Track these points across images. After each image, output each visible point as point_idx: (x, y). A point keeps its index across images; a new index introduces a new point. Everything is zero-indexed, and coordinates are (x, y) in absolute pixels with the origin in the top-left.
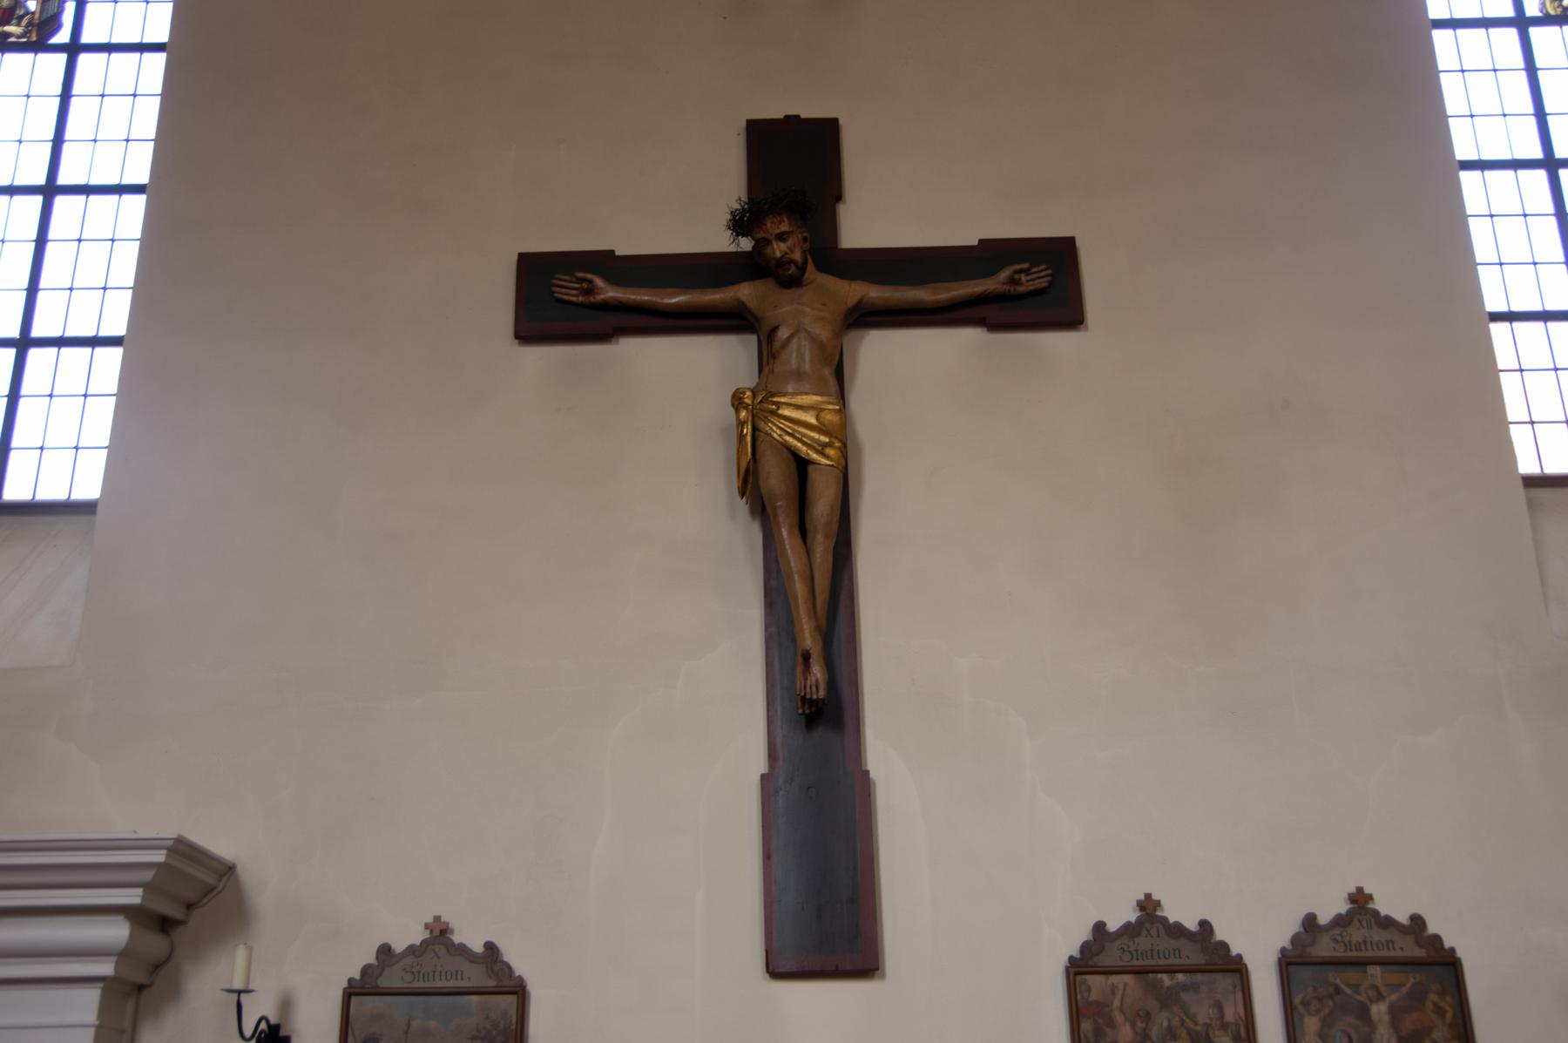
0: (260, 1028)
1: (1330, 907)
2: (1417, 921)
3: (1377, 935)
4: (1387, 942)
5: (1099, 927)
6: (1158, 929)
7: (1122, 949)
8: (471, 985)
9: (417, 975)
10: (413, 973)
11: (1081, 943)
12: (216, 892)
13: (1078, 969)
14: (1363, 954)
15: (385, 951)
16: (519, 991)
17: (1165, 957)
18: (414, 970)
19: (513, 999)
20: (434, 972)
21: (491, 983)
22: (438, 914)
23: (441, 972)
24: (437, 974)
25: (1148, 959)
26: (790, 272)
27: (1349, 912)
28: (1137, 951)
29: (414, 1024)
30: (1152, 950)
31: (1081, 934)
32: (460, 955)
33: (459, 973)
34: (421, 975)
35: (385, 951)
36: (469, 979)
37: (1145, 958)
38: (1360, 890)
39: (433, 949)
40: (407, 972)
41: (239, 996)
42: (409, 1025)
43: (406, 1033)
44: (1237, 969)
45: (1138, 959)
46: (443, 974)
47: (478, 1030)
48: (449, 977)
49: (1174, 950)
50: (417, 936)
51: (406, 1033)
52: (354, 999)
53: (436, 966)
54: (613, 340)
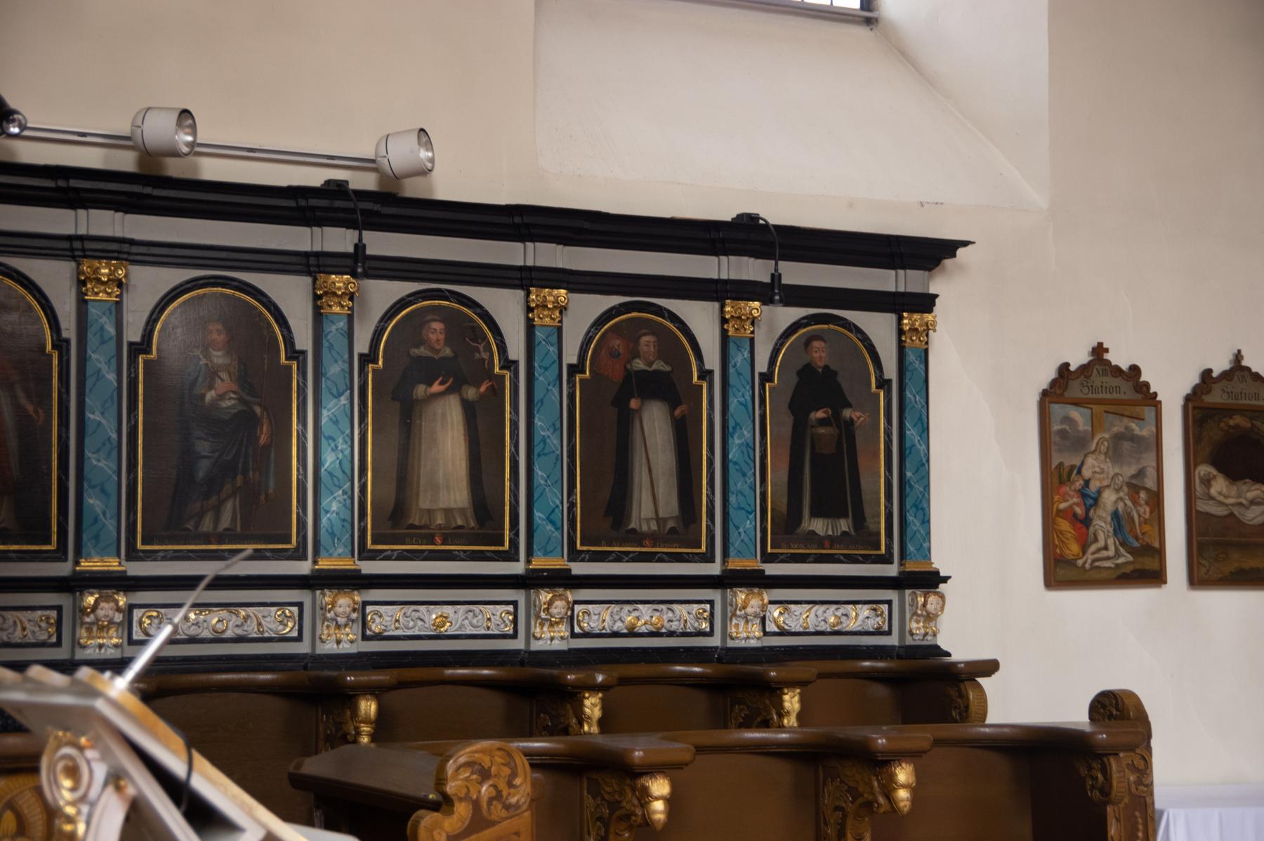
1: (1078, 357)
2: (1135, 370)
3: (1111, 381)
5: (1064, 368)
6: (1097, 369)
7: (1223, 390)
9: (1090, 388)
12: (598, 324)
13: (1049, 397)
17: (1110, 393)
18: (1229, 391)
20: (1241, 393)
23: (1106, 387)
26: (40, 423)
27: (1090, 363)
28: (1092, 386)
30: (1102, 387)
31: (1047, 374)
33: (1118, 389)
34: (1104, 388)
36: (1125, 393)
37: (1247, 398)
40: (1225, 392)
44: (1151, 400)
48: (1111, 391)
49: (1116, 387)
54: (914, 773)
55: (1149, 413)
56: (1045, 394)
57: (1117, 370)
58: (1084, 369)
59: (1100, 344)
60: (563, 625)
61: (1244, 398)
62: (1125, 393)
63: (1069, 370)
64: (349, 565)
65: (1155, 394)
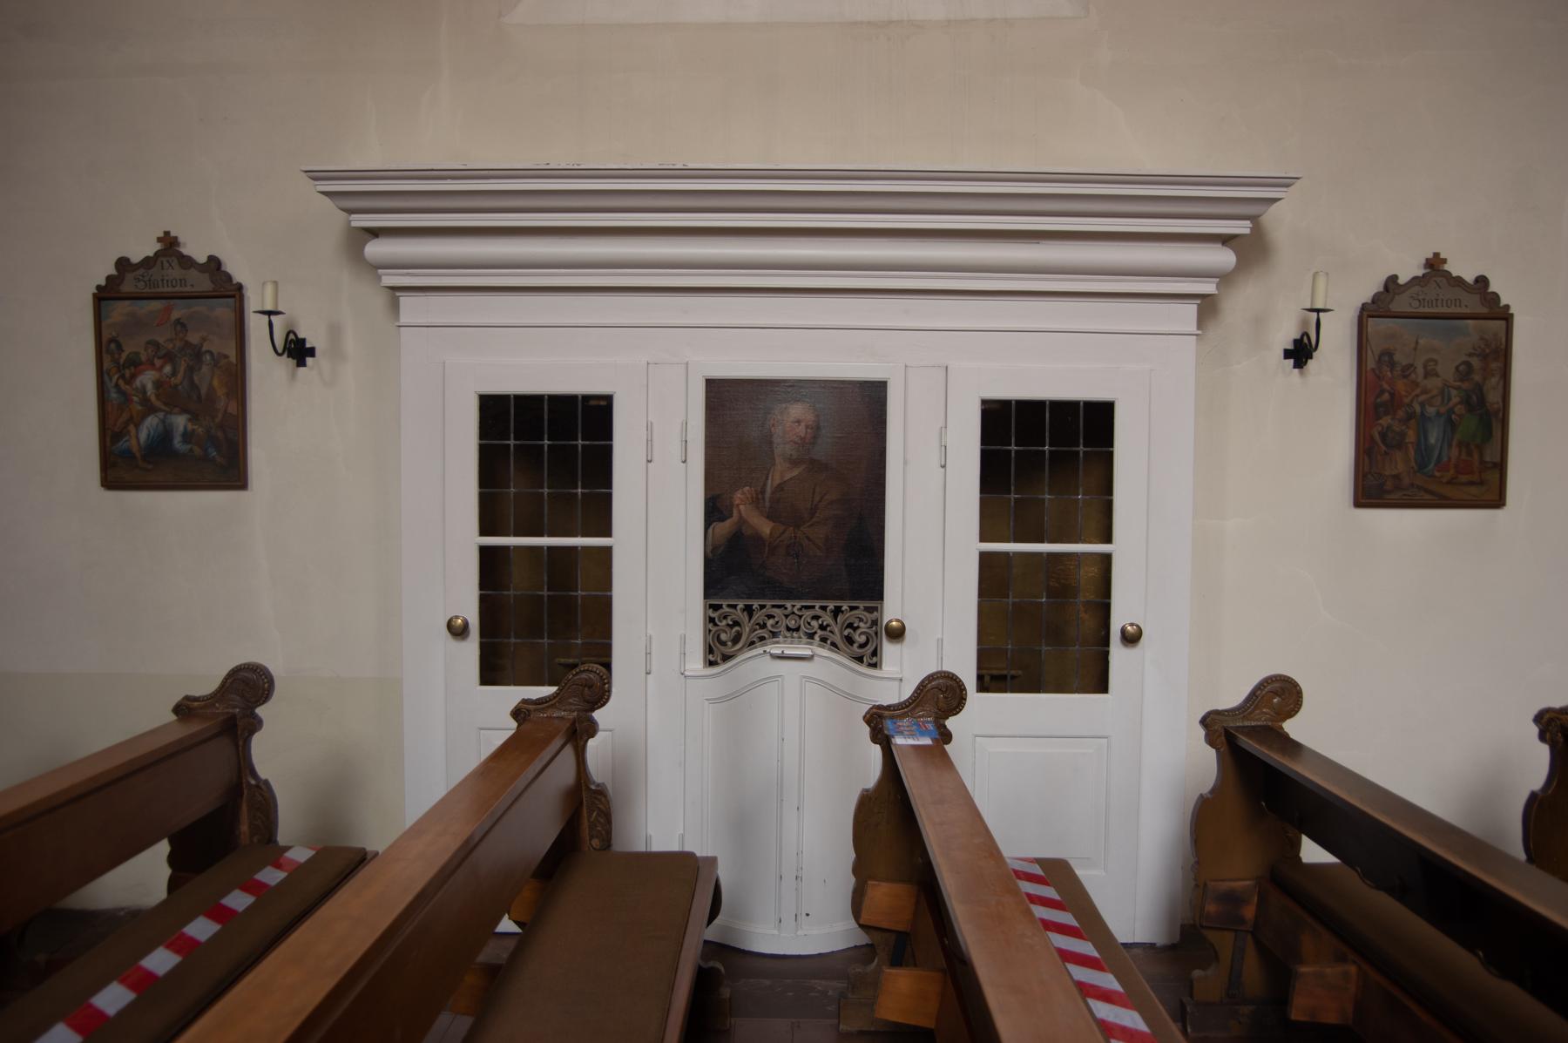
0: (290, 338)
1: (1409, 268)
2: (1482, 281)
4: (181, 280)
5: (1392, 279)
8: (1469, 311)
10: (144, 281)
11: (1373, 293)
13: (104, 296)
14: (160, 290)
15: (123, 264)
16: (1506, 316)
18: (1420, 298)
19: (1503, 323)
20: (1437, 300)
21: (1485, 310)
22: (167, 230)
23: (1442, 300)
24: (1439, 302)
25: (1437, 306)
28: (150, 280)
29: (1421, 341)
32: (1459, 286)
33: (183, 282)
34: (165, 282)
35: (123, 264)
38: (1436, 255)
39: (1435, 281)
41: (1318, 315)
42: (1417, 343)
43: (1415, 349)
45: (1424, 307)
46: (1445, 302)
47: (1474, 349)
49: (181, 280)
50: (150, 248)
51: (1415, 349)
52: (104, 303)
53: (1438, 295)
55: (222, 311)
56: (1364, 307)
57: (1459, 281)
58: (147, 262)
59: (1436, 255)
60: (780, 487)
61: (165, 285)
62: (1466, 306)
63: (1398, 284)
64: (1363, 468)
65: (1507, 307)
